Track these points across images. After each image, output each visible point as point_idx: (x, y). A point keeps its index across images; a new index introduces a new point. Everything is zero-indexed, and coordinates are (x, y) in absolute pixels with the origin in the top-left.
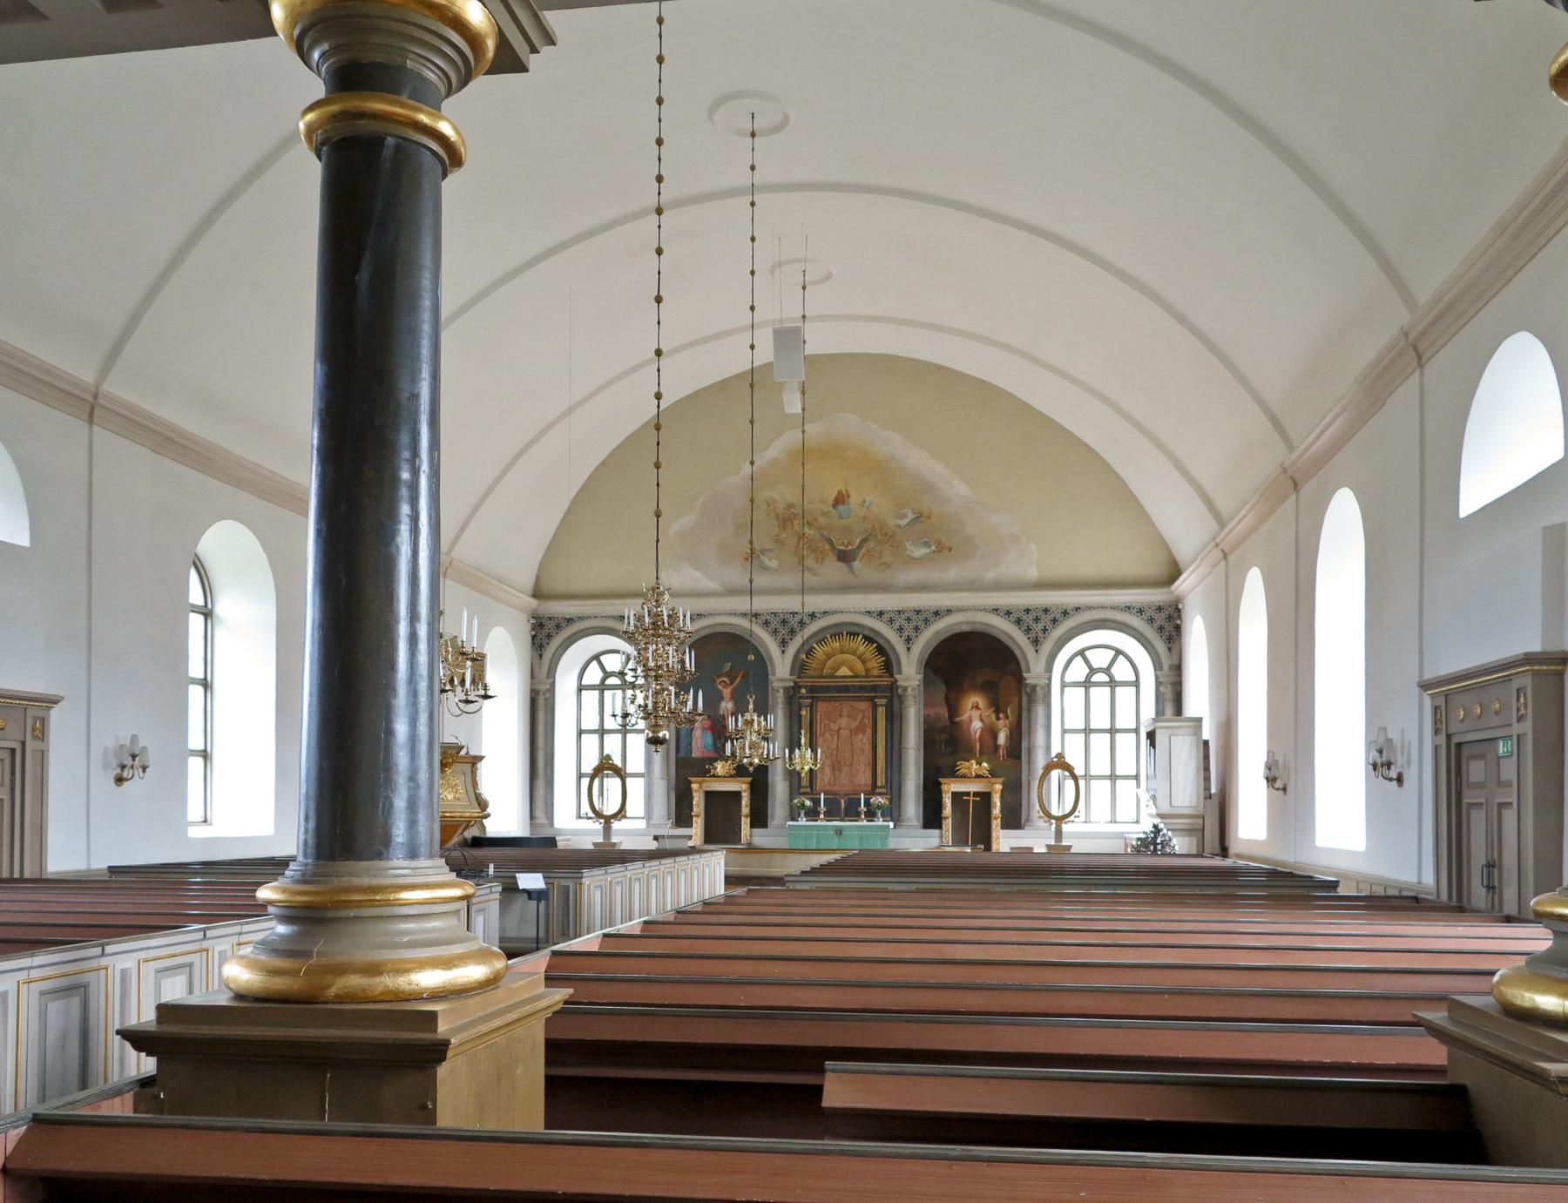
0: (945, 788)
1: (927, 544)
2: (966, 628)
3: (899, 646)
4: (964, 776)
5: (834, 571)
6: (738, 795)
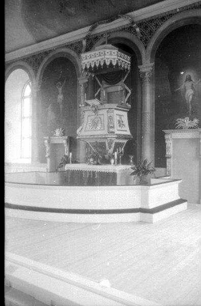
0: (166, 137)
2: (182, 24)
4: (181, 128)
6: (62, 144)
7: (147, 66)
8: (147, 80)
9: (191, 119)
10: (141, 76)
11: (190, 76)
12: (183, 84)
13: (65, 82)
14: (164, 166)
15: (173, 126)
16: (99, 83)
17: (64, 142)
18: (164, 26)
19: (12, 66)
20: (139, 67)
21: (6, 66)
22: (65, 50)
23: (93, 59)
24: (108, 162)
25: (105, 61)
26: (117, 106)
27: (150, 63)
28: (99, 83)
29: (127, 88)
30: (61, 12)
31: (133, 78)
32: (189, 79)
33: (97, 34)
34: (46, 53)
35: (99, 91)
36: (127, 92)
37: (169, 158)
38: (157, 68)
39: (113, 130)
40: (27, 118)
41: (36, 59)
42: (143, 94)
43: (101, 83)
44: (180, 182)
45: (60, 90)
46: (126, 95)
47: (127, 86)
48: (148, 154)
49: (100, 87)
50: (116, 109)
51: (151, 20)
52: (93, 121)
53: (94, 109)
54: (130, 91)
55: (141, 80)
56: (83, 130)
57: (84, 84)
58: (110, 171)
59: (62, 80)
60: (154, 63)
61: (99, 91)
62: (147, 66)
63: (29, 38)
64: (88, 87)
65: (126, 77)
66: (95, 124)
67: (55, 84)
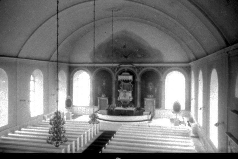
1: (141, 55)
3: (136, 74)
5: (124, 59)
6: (106, 100)
7: (138, 79)
15: (146, 97)
17: (107, 99)
21: (232, 152)
22: (106, 68)
27: (123, 102)
32: (151, 85)
34: (99, 67)
38: (141, 80)
39: (89, 131)
40: (32, 80)
42: (137, 87)
51: (140, 67)
62: (138, 79)
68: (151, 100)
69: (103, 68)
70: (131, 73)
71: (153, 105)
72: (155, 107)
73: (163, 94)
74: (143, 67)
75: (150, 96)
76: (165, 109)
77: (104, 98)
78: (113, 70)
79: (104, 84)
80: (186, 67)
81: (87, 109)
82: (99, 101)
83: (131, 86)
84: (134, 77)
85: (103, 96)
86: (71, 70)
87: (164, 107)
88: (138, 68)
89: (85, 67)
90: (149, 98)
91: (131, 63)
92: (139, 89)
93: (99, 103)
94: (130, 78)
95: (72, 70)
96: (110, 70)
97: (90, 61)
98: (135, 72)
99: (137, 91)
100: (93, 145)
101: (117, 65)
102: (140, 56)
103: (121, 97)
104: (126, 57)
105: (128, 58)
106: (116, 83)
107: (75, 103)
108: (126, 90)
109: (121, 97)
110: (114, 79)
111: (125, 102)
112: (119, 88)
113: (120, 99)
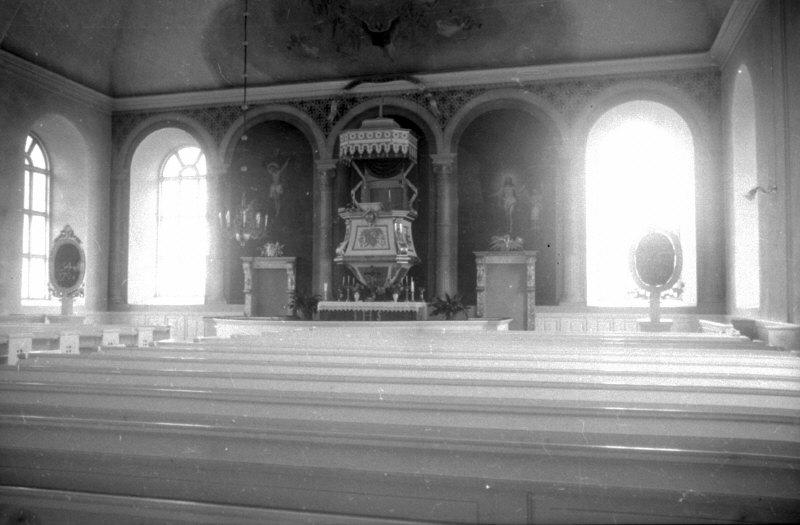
0: (479, 261)
3: (436, 128)
4: (499, 250)
5: (371, 55)
8: (445, 177)
9: (514, 238)
10: (435, 170)
11: (511, 179)
12: (502, 189)
13: (286, 164)
14: (474, 302)
15: (487, 247)
16: (360, 173)
17: (290, 266)
18: (472, 104)
19: (160, 118)
20: (432, 156)
23: (378, 141)
24: (390, 299)
25: (392, 146)
26: (408, 215)
28: (360, 173)
29: (411, 185)
30: (289, 48)
31: (420, 169)
32: (509, 183)
33: (356, 94)
35: (358, 186)
36: (410, 193)
37: (481, 291)
41: (219, 116)
43: (363, 172)
44: (509, 321)
45: (276, 176)
46: (410, 197)
47: (412, 182)
48: (447, 286)
49: (361, 179)
50: (405, 218)
51: (452, 91)
52: (366, 234)
53: (372, 216)
54: (416, 191)
55: (436, 175)
56: (350, 248)
57: (329, 172)
58: (337, 309)
59: (281, 160)
60: (456, 154)
61: (358, 186)
62: (444, 156)
63: (209, 77)
64: (335, 178)
65: (408, 171)
66: (371, 238)
67: (264, 165)
68: (509, 260)
69: (269, 109)
70: (404, 121)
71: (524, 289)
72: (531, 298)
73: (573, 217)
74: (471, 92)
75: (507, 241)
76: (590, 303)
77: (275, 260)
78: (319, 118)
79: (277, 189)
80: (698, 75)
81: (192, 323)
82: (248, 275)
83: (410, 193)
84: (424, 140)
85: (269, 249)
86: (121, 130)
87: (583, 294)
88: (443, 100)
89: (185, 111)
90: (498, 251)
91: (406, 73)
92: (447, 207)
93: (247, 287)
94: (401, 141)
95: (126, 132)
96: (303, 116)
97: (209, 77)
98: (426, 117)
99: (437, 219)
100: (226, 330)
101: (334, 87)
102: (450, 30)
103: (354, 248)
104: (380, 40)
105: (391, 47)
106: (332, 183)
107: (138, 290)
108: (376, 206)
109: (354, 248)
110: (322, 148)
111: (376, 272)
112: (346, 202)
113: (350, 252)
